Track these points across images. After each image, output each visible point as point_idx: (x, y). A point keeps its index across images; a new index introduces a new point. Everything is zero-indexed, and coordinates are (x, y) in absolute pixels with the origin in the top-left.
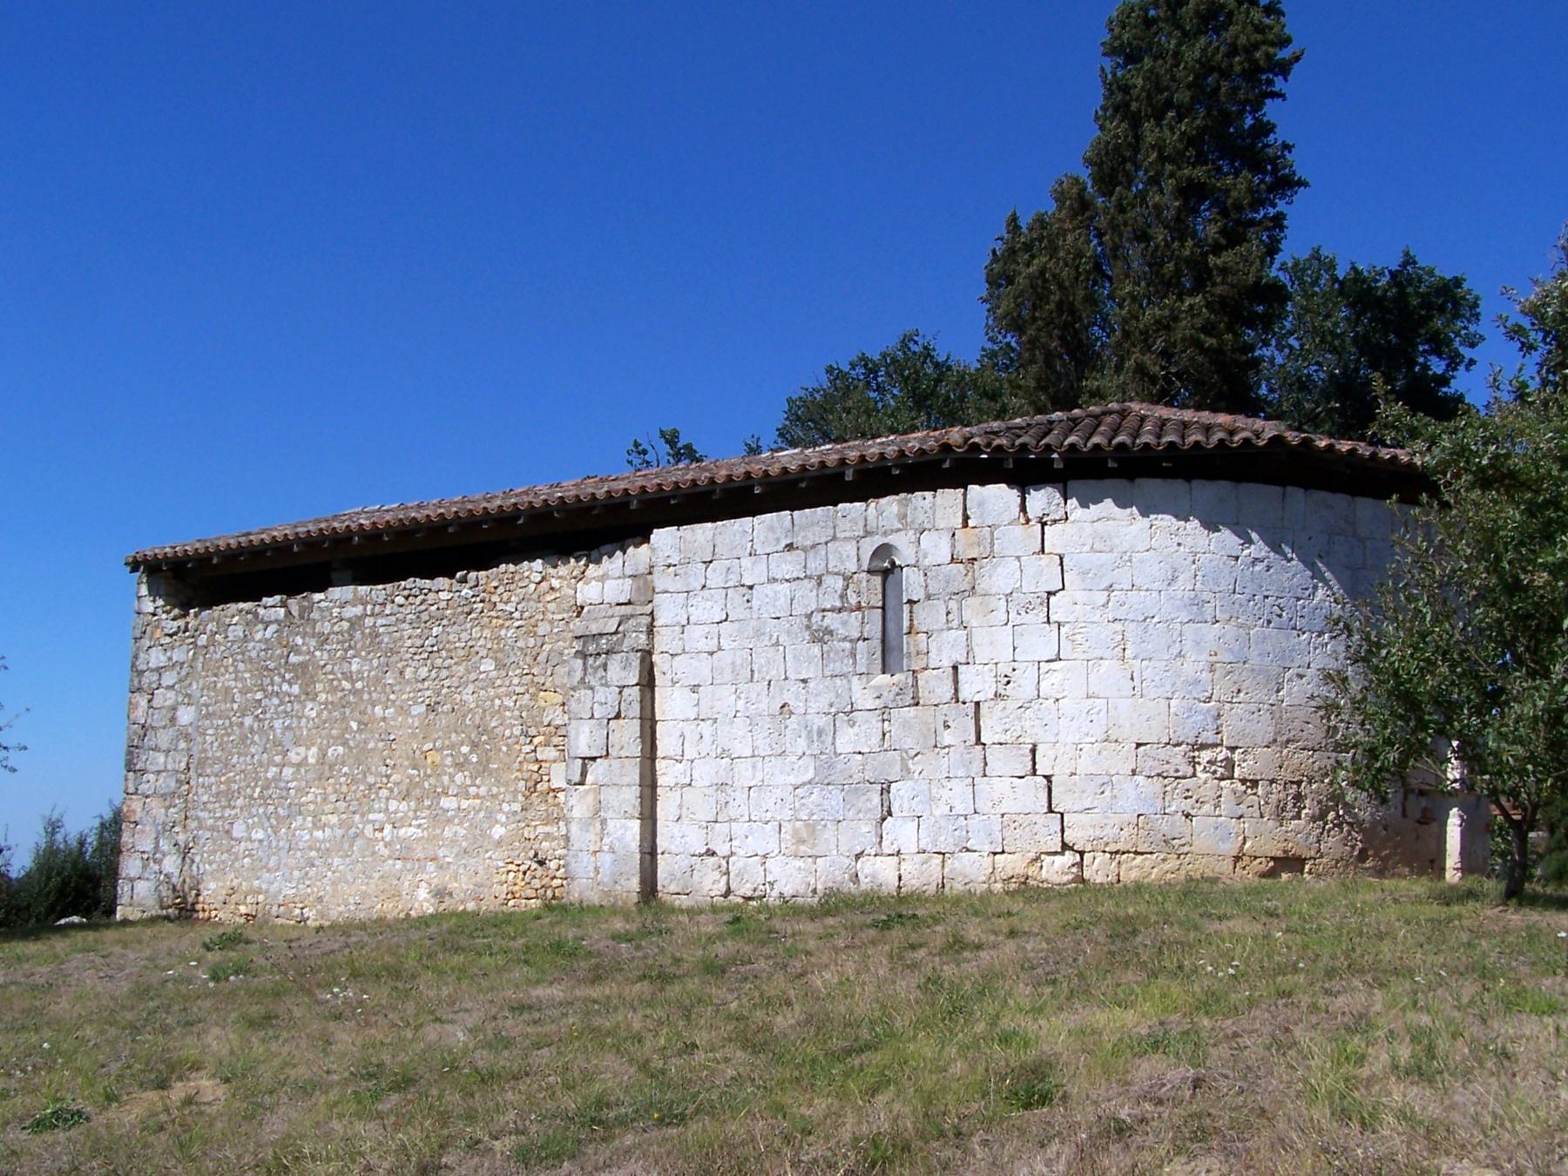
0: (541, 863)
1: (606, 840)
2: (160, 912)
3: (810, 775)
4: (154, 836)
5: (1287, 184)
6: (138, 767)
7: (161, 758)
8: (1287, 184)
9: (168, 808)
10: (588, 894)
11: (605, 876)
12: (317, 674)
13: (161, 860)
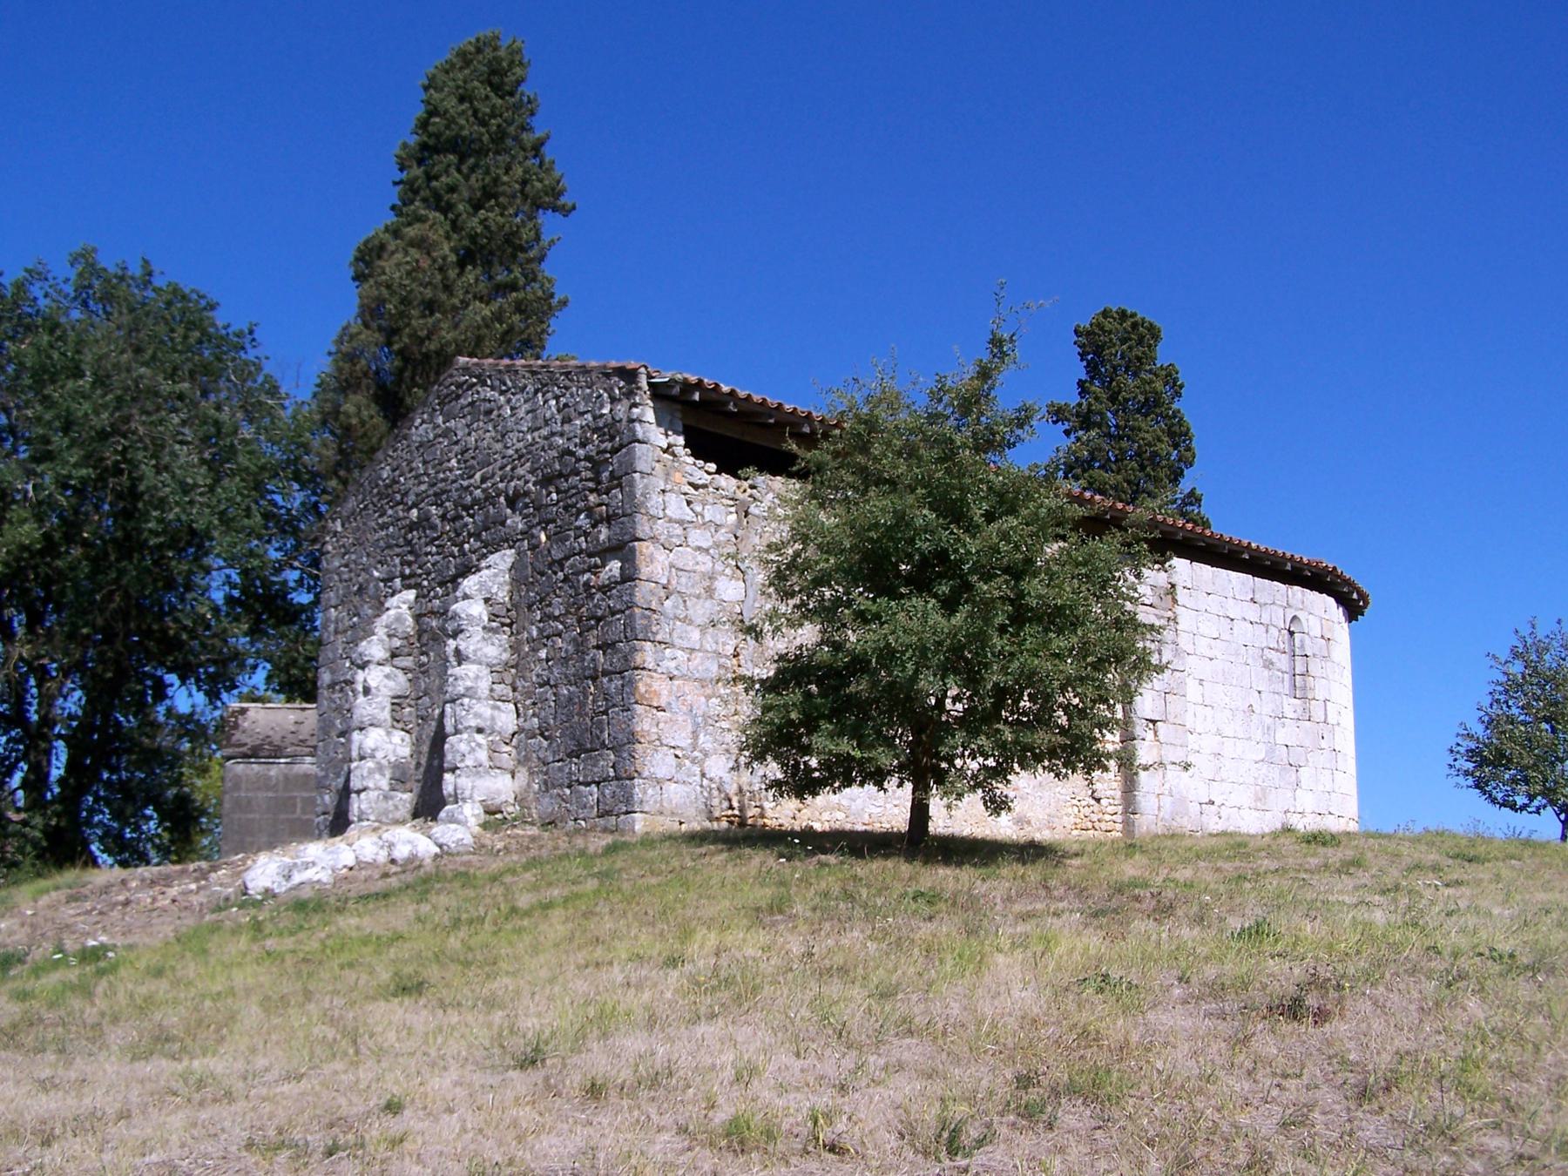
0: (1098, 800)
1: (1167, 786)
2: (707, 824)
3: (1262, 756)
4: (690, 728)
5: (550, 199)
6: (659, 638)
7: (695, 635)
8: (550, 199)
9: (708, 698)
10: (1153, 827)
11: (1166, 813)
12: (266, 551)
13: (703, 761)
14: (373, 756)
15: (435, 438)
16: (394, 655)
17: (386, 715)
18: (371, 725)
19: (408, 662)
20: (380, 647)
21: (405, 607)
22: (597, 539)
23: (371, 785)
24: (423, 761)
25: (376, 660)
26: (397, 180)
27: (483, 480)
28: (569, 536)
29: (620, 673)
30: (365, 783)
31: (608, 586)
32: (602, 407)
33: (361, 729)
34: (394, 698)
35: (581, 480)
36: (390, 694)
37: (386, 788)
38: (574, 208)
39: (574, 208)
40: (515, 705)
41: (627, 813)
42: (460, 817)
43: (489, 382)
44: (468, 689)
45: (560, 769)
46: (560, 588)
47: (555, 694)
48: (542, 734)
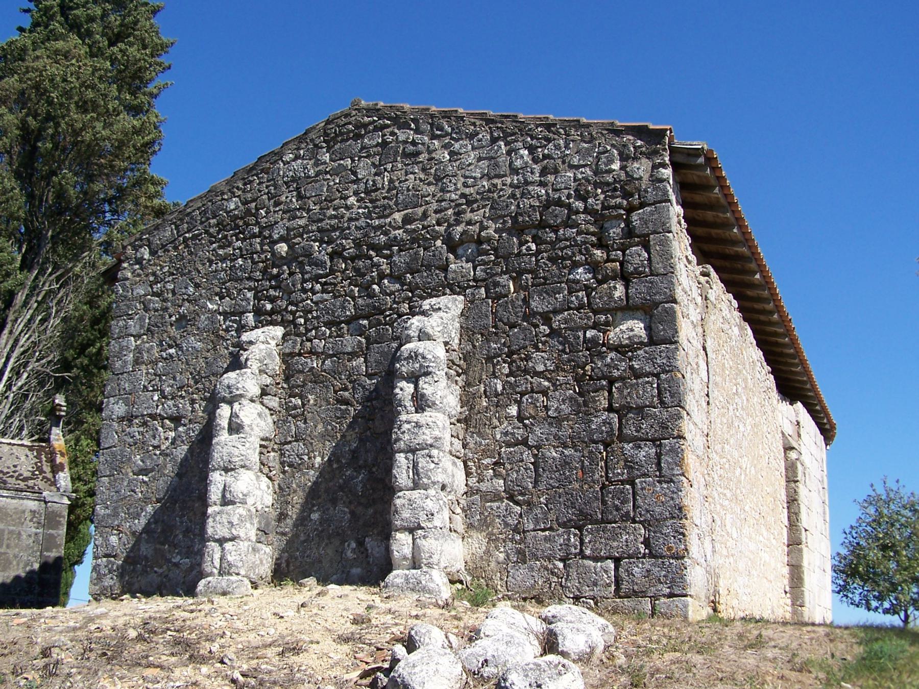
14: (244, 502)
15: (317, 176)
16: (264, 393)
17: (255, 458)
18: (242, 467)
19: (273, 402)
20: (254, 381)
21: (273, 343)
22: (611, 296)
23: (242, 535)
24: (293, 513)
25: (249, 395)
26: (26, 8)
27: (407, 220)
28: (561, 288)
29: (653, 440)
30: (235, 532)
31: (627, 346)
32: (611, 161)
33: (226, 470)
34: (262, 439)
35: (578, 233)
36: (262, 435)
37: (254, 538)
38: (169, 68)
39: (169, 68)
40: (465, 463)
41: (671, 595)
42: (431, 585)
43: (413, 126)
44: (437, 439)
45: (547, 539)
46: (544, 343)
47: (535, 456)
48: (511, 498)
